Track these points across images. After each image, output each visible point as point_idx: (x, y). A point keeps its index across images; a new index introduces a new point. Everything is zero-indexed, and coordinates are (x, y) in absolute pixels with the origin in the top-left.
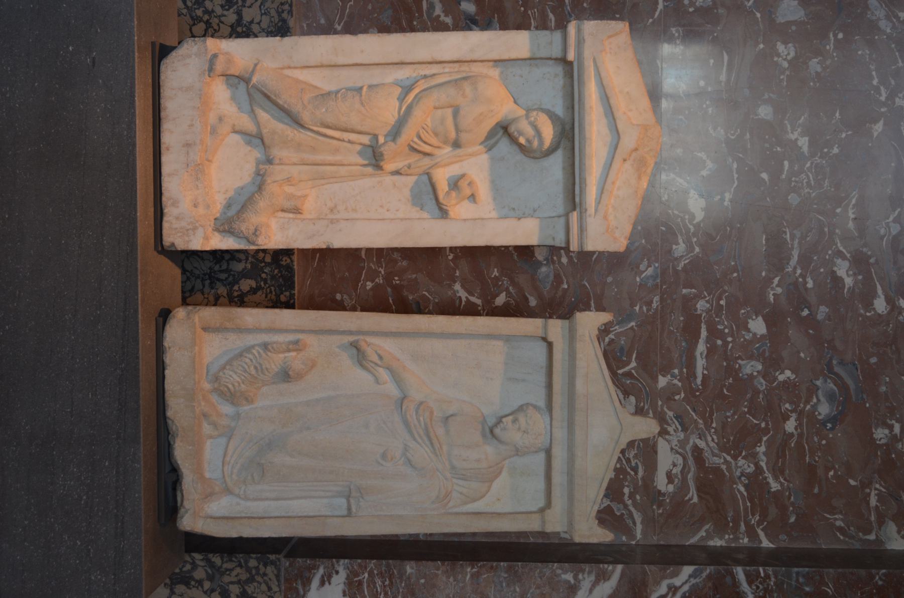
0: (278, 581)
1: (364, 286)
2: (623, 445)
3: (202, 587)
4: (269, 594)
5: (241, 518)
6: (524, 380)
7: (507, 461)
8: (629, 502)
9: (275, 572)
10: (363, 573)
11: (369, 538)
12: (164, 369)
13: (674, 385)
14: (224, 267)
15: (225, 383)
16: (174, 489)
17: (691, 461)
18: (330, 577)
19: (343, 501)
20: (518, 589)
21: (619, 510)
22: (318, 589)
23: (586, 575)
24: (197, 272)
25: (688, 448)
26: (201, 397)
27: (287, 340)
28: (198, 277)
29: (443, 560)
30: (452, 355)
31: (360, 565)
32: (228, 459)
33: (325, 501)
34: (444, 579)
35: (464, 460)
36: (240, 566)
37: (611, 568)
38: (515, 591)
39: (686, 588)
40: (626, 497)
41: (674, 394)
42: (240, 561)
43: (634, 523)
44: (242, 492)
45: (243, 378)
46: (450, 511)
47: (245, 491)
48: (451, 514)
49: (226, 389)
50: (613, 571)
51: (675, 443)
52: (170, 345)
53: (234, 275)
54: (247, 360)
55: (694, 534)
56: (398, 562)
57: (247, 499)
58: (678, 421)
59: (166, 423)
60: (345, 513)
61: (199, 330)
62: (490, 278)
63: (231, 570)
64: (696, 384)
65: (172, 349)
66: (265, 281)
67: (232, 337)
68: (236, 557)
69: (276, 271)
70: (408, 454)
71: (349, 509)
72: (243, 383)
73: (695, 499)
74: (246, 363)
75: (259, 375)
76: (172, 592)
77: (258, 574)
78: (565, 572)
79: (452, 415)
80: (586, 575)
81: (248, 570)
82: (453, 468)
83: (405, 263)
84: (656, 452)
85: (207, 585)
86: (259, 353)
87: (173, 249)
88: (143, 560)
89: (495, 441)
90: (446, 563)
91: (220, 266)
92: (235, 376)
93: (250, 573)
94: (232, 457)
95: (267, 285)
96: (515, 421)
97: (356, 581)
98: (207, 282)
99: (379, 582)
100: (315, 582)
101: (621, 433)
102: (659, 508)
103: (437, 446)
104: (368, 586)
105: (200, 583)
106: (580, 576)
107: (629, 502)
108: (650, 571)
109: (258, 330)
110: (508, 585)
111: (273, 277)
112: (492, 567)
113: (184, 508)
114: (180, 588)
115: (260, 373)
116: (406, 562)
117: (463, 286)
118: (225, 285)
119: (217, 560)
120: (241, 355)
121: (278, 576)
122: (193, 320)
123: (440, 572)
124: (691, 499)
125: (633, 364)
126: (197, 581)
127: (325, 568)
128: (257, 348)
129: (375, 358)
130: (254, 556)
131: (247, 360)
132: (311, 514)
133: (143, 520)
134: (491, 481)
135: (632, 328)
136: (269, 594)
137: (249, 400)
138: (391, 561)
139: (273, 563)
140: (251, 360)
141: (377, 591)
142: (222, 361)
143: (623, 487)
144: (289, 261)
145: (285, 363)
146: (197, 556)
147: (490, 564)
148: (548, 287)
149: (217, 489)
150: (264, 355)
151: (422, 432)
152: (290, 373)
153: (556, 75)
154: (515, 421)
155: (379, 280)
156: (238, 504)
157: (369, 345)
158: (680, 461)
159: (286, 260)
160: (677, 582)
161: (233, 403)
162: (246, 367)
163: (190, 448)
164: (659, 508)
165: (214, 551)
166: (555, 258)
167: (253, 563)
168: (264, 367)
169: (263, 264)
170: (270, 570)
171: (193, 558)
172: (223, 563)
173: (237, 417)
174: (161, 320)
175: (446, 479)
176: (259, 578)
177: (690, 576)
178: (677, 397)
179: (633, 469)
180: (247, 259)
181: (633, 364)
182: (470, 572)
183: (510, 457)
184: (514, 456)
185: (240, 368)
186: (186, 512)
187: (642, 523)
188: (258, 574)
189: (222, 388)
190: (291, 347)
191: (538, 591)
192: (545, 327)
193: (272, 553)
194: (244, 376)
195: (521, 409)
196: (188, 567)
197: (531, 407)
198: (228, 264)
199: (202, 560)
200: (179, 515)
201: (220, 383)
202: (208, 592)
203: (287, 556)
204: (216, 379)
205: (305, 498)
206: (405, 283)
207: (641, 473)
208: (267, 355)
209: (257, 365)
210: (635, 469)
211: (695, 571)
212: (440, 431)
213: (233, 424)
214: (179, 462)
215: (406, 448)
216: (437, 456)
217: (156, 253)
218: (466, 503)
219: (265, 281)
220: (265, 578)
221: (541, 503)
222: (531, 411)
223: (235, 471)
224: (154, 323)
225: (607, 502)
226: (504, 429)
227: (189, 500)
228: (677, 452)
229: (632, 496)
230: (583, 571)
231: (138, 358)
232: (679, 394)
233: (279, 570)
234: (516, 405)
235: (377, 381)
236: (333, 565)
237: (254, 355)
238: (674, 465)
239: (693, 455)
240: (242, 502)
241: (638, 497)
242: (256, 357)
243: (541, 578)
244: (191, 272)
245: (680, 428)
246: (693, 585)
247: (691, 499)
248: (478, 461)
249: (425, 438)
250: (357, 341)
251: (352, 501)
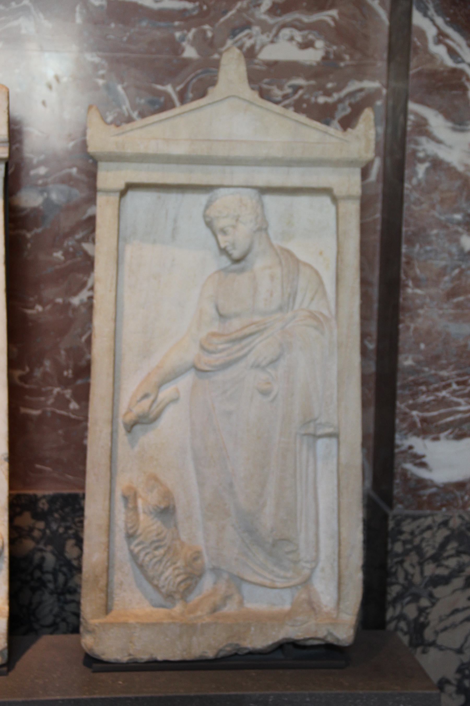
0: (419, 517)
1: (74, 411)
2: (255, 96)
3: (426, 608)
4: (435, 529)
5: (339, 566)
6: (175, 221)
7: (275, 242)
8: (336, 96)
9: (409, 521)
10: (412, 417)
11: (372, 410)
12: (156, 662)
13: (194, 37)
14: (49, 577)
16: (305, 647)
17: (288, 18)
18: (416, 456)
19: (321, 443)
20: (435, 232)
21: (344, 109)
22: (430, 470)
23: (420, 148)
24: (56, 610)
25: (271, 21)
26: (192, 616)
27: (123, 510)
28: (62, 609)
29: (397, 322)
31: (403, 420)
32: (268, 582)
33: (320, 464)
34: (420, 320)
35: (271, 295)
36: (401, 562)
37: (411, 117)
38: (437, 235)
39: (440, 21)
40: (330, 100)
41: (205, 38)
42: (397, 563)
43: (361, 90)
44: (308, 565)
45: (169, 564)
46: (333, 312)
47: (307, 562)
48: (337, 312)
50: (416, 114)
51: (264, 38)
53: (61, 566)
54: (147, 559)
55: (377, 15)
56: (400, 375)
57: (316, 560)
58: (239, 33)
59: (224, 658)
60: (334, 441)
61: (109, 618)
62: (65, 262)
63: (407, 573)
64: (194, 9)
65: (131, 652)
66: (67, 528)
67: (117, 577)
68: (392, 567)
69: (56, 515)
70: (264, 363)
71: (330, 435)
72: (175, 563)
73: (334, 13)
76: (433, 644)
77: (411, 542)
78: (415, 173)
79: (217, 309)
80: (420, 148)
81: (406, 553)
82: (281, 309)
83: (47, 363)
84: (276, 63)
85: (424, 602)
86: (138, 544)
87: (6, 652)
88: (389, 692)
89: (250, 257)
90: (401, 317)
91: (49, 581)
92: (167, 573)
93: (410, 550)
94: (265, 577)
95: (73, 526)
96: (224, 232)
97: (422, 425)
98: (69, 597)
99: (423, 398)
100: (422, 473)
101: (239, 98)
102: (342, 59)
103: (253, 329)
104: (428, 410)
105: (422, 610)
106: (421, 155)
107: (336, 96)
108: (417, 67)
109: (109, 546)
110: (429, 243)
111: (63, 519)
112: (408, 263)
113: (325, 637)
114: (428, 634)
115: (163, 543)
116: (400, 366)
117: (75, 294)
118: (72, 576)
119: (394, 590)
120: (141, 567)
121: (415, 518)
122: (96, 626)
123: (412, 326)
124: (334, 19)
125: (169, 88)
126: (420, 615)
127: (405, 462)
128: (132, 547)
129: (146, 403)
130: (390, 546)
131: (147, 559)
132: (335, 482)
133: (339, 691)
134: (297, 262)
135: (125, 89)
136: (435, 529)
137: (197, 556)
138: (399, 384)
139: (398, 524)
140: (147, 554)
141: (434, 400)
142: (149, 588)
143: (316, 104)
144: (44, 501)
146: (390, 613)
147: (403, 266)
148: (75, 191)
149: (304, 596)
150: (141, 538)
151: (237, 347)
152: (162, 506)
153: (405, 299)
154: (224, 232)
155: (68, 393)
156: (323, 570)
157: (129, 411)
158: (286, 32)
159: (43, 504)
160: (431, 32)
161: (200, 576)
162: (155, 560)
164: (342, 59)
165: (384, 593)
166: (40, 182)
167: (398, 548)
168: (155, 538)
169: (48, 532)
170: (407, 527)
171: (393, 619)
172: (397, 583)
173: (216, 570)
174: (96, 666)
175: (294, 317)
176: (417, 541)
177: (425, 15)
178: (209, 34)
179: (295, 92)
180: (41, 550)
181: (169, 88)
182: (413, 289)
183: (268, 238)
184: (267, 234)
186: (330, 634)
187: (361, 80)
188: (411, 542)
189: (181, 590)
190: (130, 506)
191: (438, 207)
192: (107, 192)
193: (386, 525)
194: (167, 562)
195: (209, 224)
196: (403, 625)
197: (208, 212)
198: (47, 572)
199: (394, 607)
200: (336, 643)
201: (175, 592)
202: (434, 601)
203: (391, 505)
204: (170, 596)
205: (315, 489)
206: (71, 363)
207: (300, 82)
208: (141, 535)
210: (296, 88)
211: (419, 9)
212: (236, 324)
213: (226, 576)
214: (270, 642)
215: (257, 366)
216: (265, 329)
217: (11, 674)
218: (324, 293)
219: (67, 528)
220: (417, 532)
221: (326, 200)
222: (212, 213)
223: (282, 573)
224: (97, 675)
225: (335, 123)
226: (234, 245)
228: (276, 35)
229: (328, 93)
230: (414, 152)
231: (137, 699)
232: (204, 32)
233: (407, 517)
234: (206, 231)
235: (175, 400)
236: (402, 452)
238: (292, 39)
239: (280, 15)
240: (321, 565)
241: (330, 85)
243: (421, 203)
244: (56, 616)
245: (247, 32)
246: (436, 11)
247: (334, 19)
248: (272, 278)
249: (244, 342)
250: (125, 425)
251: (320, 432)
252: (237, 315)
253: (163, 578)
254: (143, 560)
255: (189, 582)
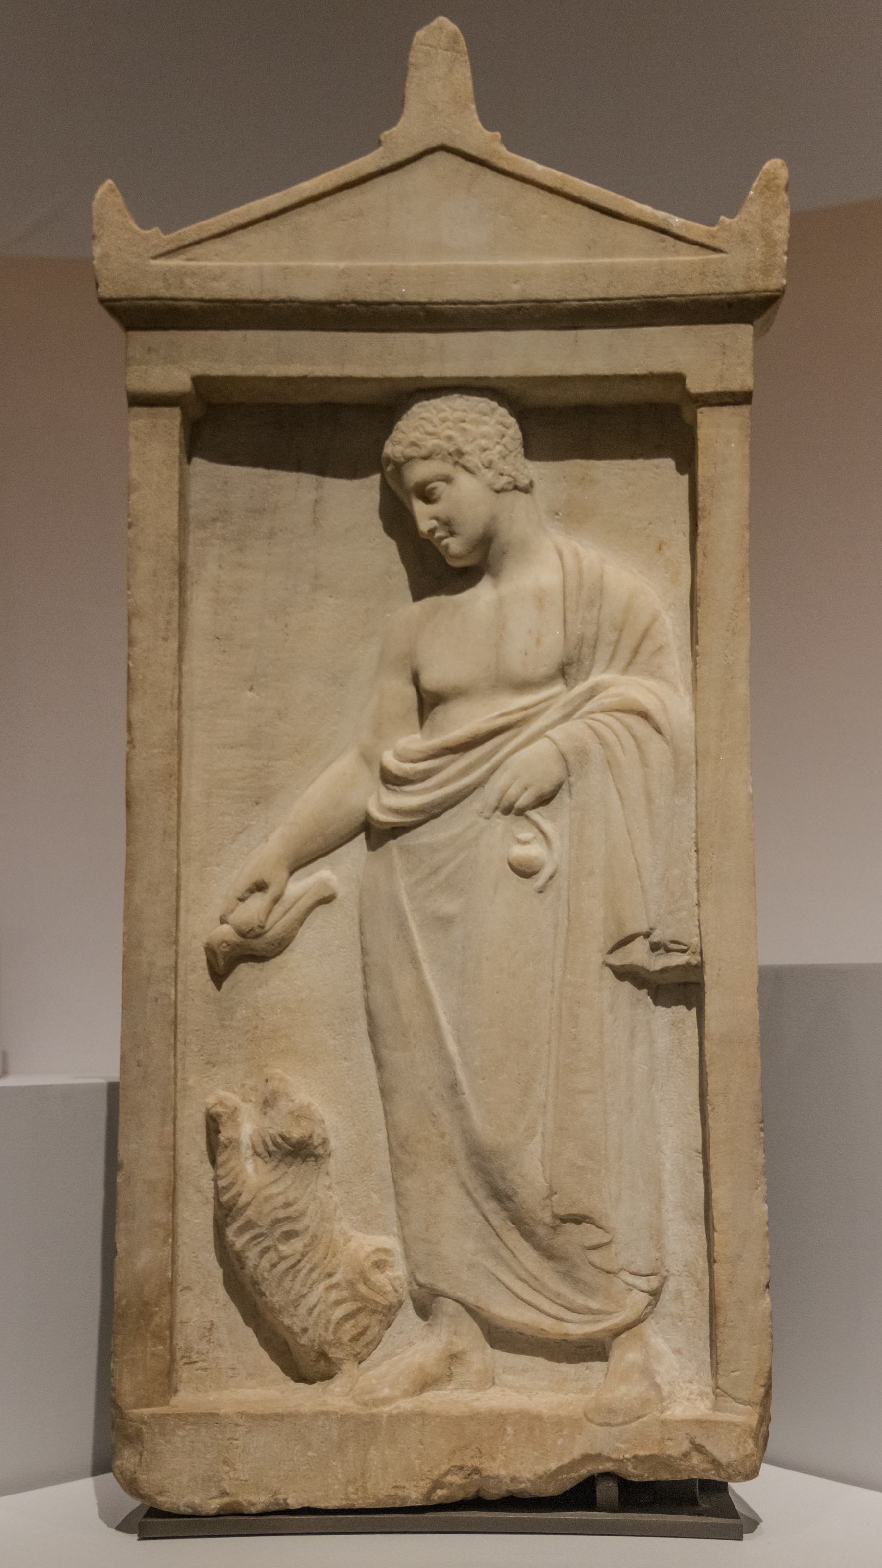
15: (331, 1328)
30: (251, 689)
45: (314, 1275)
49: (348, 1326)
52: (214, 1493)
54: (265, 1263)
65: (226, 1485)
74: (274, 1266)
75: (307, 1229)
86: (242, 1230)
129: (258, 903)
131: (265, 1263)
145: (270, 1153)
154: (427, 495)
156: (678, 1295)
162: (283, 1266)
163: (509, 1429)
185: (287, 1283)
194: (312, 1270)
208: (248, 1205)
209: (278, 1232)
227: (662, 1440)
237: (249, 1242)
242: (255, 1238)
252: (403, 432)
253: (302, 1310)
254: (256, 1266)
255: (363, 1320)
